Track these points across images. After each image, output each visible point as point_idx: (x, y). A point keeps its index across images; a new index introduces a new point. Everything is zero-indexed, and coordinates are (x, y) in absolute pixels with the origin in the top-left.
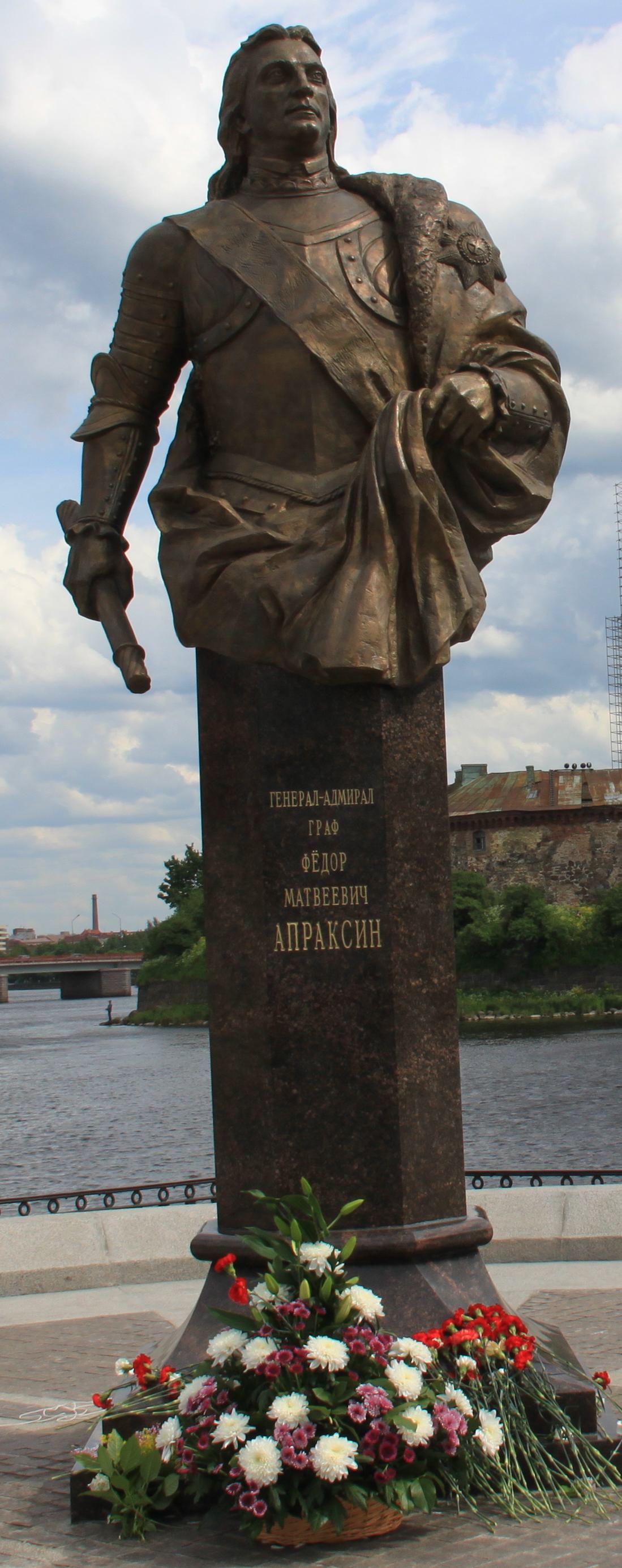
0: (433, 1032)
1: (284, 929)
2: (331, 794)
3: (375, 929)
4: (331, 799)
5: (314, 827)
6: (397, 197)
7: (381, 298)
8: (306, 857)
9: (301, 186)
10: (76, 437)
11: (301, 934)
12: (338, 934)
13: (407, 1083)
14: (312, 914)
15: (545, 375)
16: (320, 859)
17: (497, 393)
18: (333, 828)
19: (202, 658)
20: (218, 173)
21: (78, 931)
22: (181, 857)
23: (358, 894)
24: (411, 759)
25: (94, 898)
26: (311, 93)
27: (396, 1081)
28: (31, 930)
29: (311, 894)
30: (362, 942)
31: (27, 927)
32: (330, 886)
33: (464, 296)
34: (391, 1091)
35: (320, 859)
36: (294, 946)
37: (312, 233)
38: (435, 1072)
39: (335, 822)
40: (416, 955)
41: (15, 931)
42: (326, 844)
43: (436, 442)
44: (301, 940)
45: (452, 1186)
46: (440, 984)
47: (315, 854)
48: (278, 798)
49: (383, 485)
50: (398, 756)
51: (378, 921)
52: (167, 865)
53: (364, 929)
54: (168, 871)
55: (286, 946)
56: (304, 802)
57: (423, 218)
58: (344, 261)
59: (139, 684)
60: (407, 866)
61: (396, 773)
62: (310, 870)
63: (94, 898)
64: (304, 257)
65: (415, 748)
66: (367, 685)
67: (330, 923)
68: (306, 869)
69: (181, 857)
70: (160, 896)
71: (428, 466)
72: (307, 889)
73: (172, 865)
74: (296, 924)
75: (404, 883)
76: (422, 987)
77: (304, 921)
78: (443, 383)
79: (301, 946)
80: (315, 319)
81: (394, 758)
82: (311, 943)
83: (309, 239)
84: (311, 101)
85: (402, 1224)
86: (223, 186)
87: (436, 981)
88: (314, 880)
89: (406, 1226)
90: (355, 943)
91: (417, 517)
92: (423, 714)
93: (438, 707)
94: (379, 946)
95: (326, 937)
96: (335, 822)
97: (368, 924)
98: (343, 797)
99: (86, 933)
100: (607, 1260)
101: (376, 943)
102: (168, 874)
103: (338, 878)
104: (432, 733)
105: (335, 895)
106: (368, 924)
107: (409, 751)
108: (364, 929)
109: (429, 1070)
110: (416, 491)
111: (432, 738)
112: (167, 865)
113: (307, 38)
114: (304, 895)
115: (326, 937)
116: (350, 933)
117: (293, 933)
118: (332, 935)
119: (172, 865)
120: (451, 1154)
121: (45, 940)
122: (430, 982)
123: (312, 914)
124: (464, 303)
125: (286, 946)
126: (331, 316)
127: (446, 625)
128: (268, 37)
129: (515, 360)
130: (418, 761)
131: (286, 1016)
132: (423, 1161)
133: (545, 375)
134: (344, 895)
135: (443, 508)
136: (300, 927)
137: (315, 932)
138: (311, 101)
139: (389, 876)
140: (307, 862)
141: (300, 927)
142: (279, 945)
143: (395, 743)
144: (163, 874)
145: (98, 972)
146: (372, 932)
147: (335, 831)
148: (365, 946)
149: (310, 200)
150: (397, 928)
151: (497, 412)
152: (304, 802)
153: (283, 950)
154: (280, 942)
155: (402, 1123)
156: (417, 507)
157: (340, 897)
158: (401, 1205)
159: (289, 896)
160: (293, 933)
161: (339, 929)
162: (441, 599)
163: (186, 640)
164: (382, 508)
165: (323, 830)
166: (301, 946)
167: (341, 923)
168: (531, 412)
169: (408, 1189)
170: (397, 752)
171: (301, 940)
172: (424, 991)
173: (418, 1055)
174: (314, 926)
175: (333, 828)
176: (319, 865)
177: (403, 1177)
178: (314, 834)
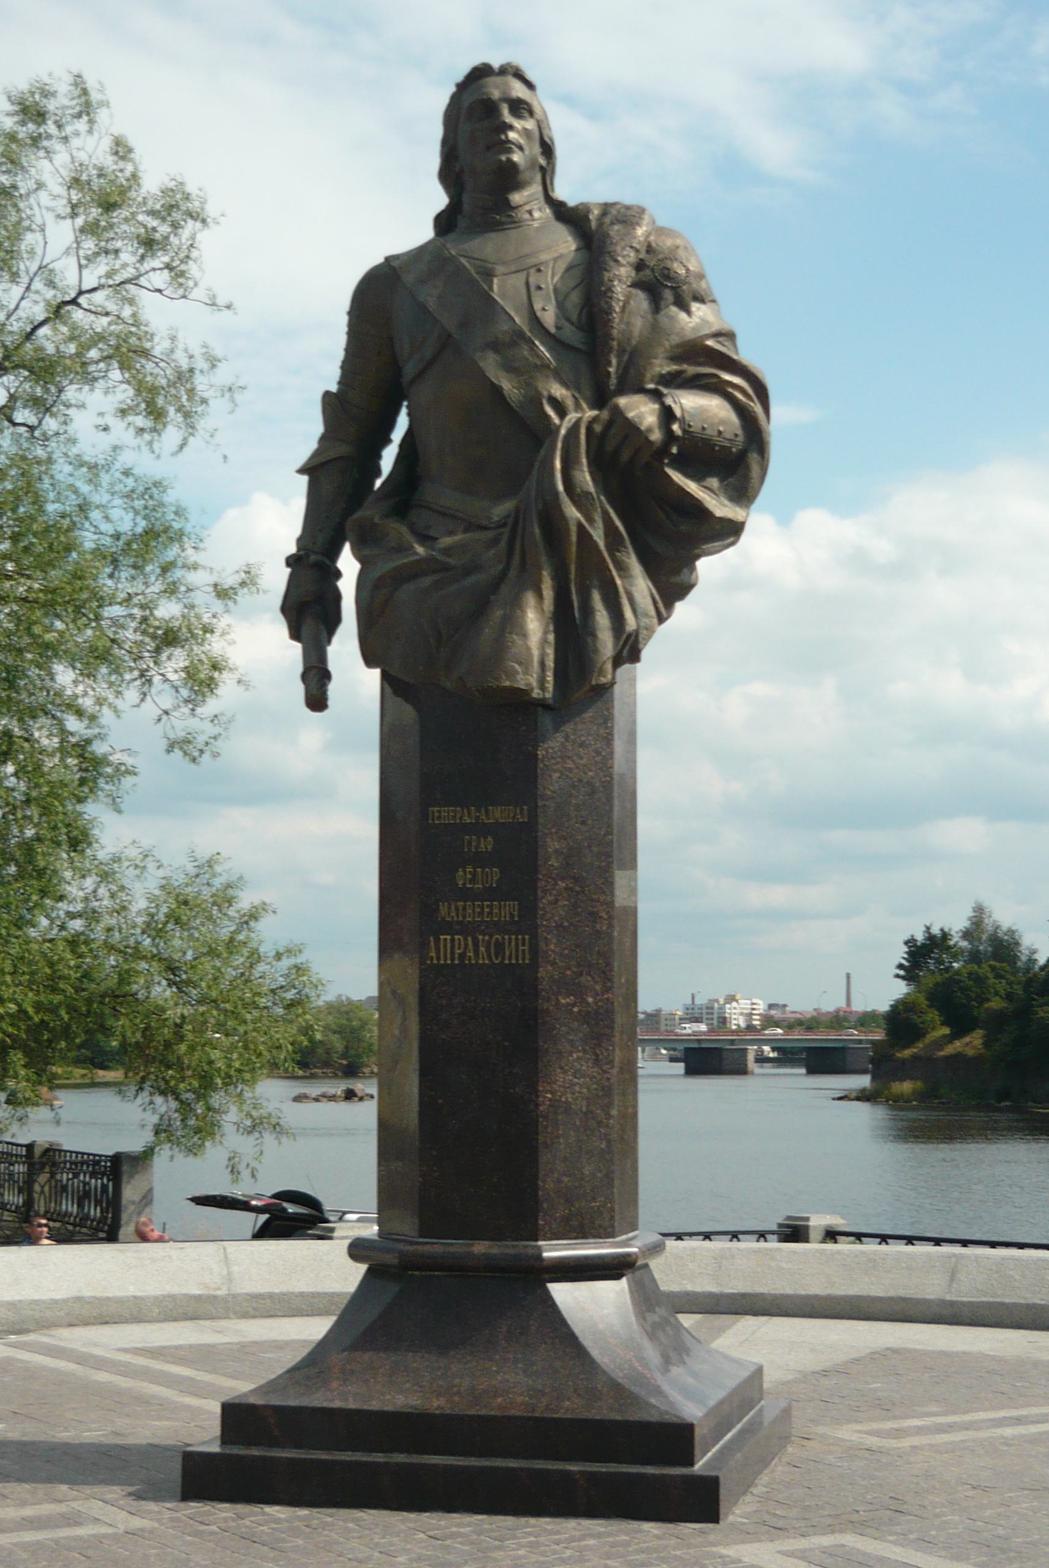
0: (584, 1050)
1: (437, 941)
2: (487, 811)
3: (524, 945)
4: (487, 815)
5: (470, 843)
6: (600, 224)
7: (567, 324)
8: (461, 873)
9: (504, 219)
10: (301, 471)
11: (453, 947)
12: (488, 949)
13: (550, 1100)
14: (465, 929)
15: (739, 396)
16: (474, 874)
17: (667, 415)
18: (487, 845)
19: (385, 677)
20: (443, 212)
21: (831, 1008)
22: (920, 937)
23: (507, 910)
24: (571, 778)
25: (848, 976)
26: (511, 127)
27: (538, 1096)
28: (785, 1006)
29: (464, 909)
30: (510, 958)
31: (781, 1002)
32: (483, 901)
33: (656, 320)
34: (532, 1106)
35: (474, 874)
36: (445, 960)
37: (504, 263)
38: (585, 1091)
39: (490, 839)
40: (568, 972)
41: (771, 1006)
42: (479, 860)
43: (600, 464)
44: (453, 953)
45: (599, 1207)
46: (596, 1003)
47: (469, 869)
48: (436, 814)
49: (540, 507)
50: (557, 775)
51: (527, 937)
52: (906, 943)
53: (513, 944)
54: (907, 950)
55: (438, 959)
56: (461, 818)
57: (616, 244)
58: (532, 289)
59: (317, 701)
60: (562, 884)
61: (554, 792)
62: (464, 884)
63: (848, 976)
64: (491, 288)
65: (577, 768)
66: (520, 703)
67: (481, 937)
68: (460, 883)
69: (920, 937)
70: (897, 976)
71: (591, 487)
72: (461, 904)
73: (910, 942)
74: (449, 937)
75: (557, 901)
76: (574, 1005)
77: (457, 934)
78: (610, 404)
79: (453, 959)
80: (495, 346)
81: (551, 776)
82: (462, 956)
83: (500, 269)
84: (512, 135)
85: (537, 1240)
86: (445, 223)
87: (590, 1000)
88: (466, 895)
89: (540, 1243)
90: (503, 958)
91: (574, 538)
92: (589, 735)
93: (607, 728)
94: (527, 962)
95: (476, 951)
96: (490, 839)
97: (517, 939)
98: (498, 814)
99: (838, 1011)
100: (929, 1323)
101: (523, 959)
102: (907, 953)
103: (491, 894)
104: (598, 753)
105: (487, 910)
106: (517, 939)
107: (570, 770)
108: (513, 944)
109: (577, 1088)
110: (572, 512)
111: (598, 759)
112: (906, 943)
113: (519, 75)
114: (457, 909)
115: (476, 951)
116: (500, 947)
117: (445, 946)
118: (482, 949)
119: (910, 942)
120: (599, 1175)
121: (799, 1016)
122: (584, 1001)
123: (465, 929)
124: (655, 328)
125: (438, 959)
126: (513, 344)
127: (606, 643)
128: (480, 73)
129: (704, 381)
130: (580, 781)
131: (436, 1028)
132: (566, 1179)
133: (739, 396)
134: (496, 911)
135: (610, 531)
136: (453, 940)
137: (466, 945)
138: (512, 135)
139: (540, 893)
140: (461, 877)
141: (453, 940)
142: (432, 958)
143: (553, 761)
144: (900, 954)
145: (843, 1048)
146: (521, 948)
147: (490, 847)
148: (514, 962)
149: (512, 233)
150: (547, 945)
151: (669, 433)
152: (461, 818)
153: (435, 962)
154: (433, 954)
155: (541, 1139)
156: (573, 529)
157: (490, 913)
158: (537, 1220)
159: (443, 910)
160: (445, 946)
161: (489, 942)
162: (602, 618)
163: (370, 661)
164: (537, 531)
165: (477, 847)
166: (453, 959)
167: (491, 936)
168: (715, 433)
169: (545, 1205)
170: (555, 771)
171: (453, 953)
172: (576, 1009)
173: (565, 1072)
174: (466, 939)
175: (487, 845)
176: (473, 881)
177: (540, 1193)
178: (470, 849)
